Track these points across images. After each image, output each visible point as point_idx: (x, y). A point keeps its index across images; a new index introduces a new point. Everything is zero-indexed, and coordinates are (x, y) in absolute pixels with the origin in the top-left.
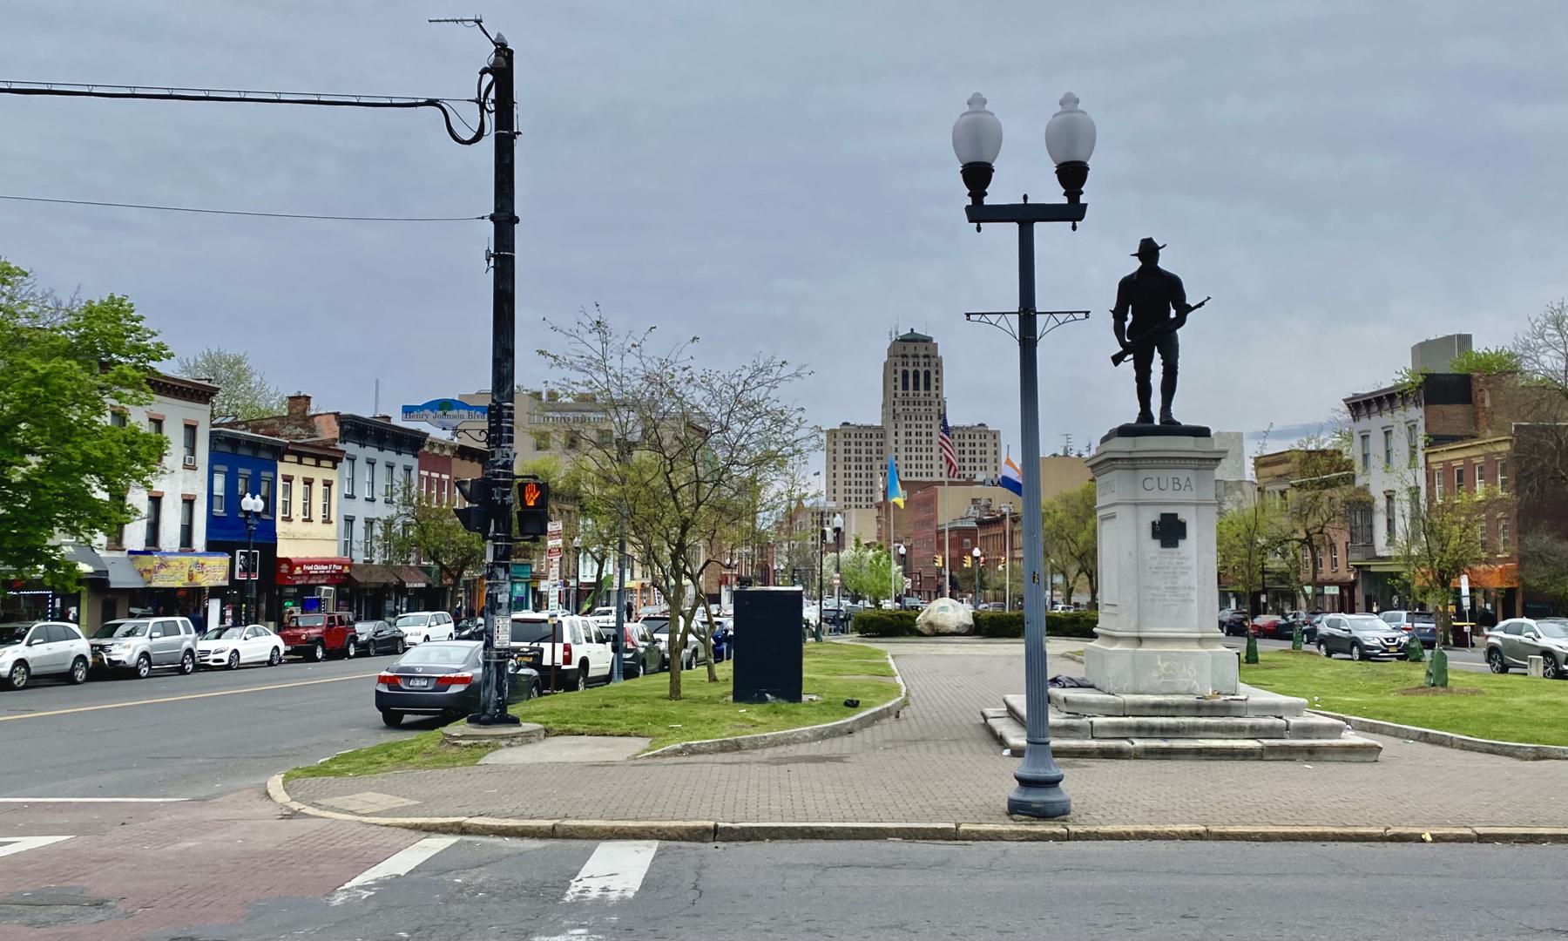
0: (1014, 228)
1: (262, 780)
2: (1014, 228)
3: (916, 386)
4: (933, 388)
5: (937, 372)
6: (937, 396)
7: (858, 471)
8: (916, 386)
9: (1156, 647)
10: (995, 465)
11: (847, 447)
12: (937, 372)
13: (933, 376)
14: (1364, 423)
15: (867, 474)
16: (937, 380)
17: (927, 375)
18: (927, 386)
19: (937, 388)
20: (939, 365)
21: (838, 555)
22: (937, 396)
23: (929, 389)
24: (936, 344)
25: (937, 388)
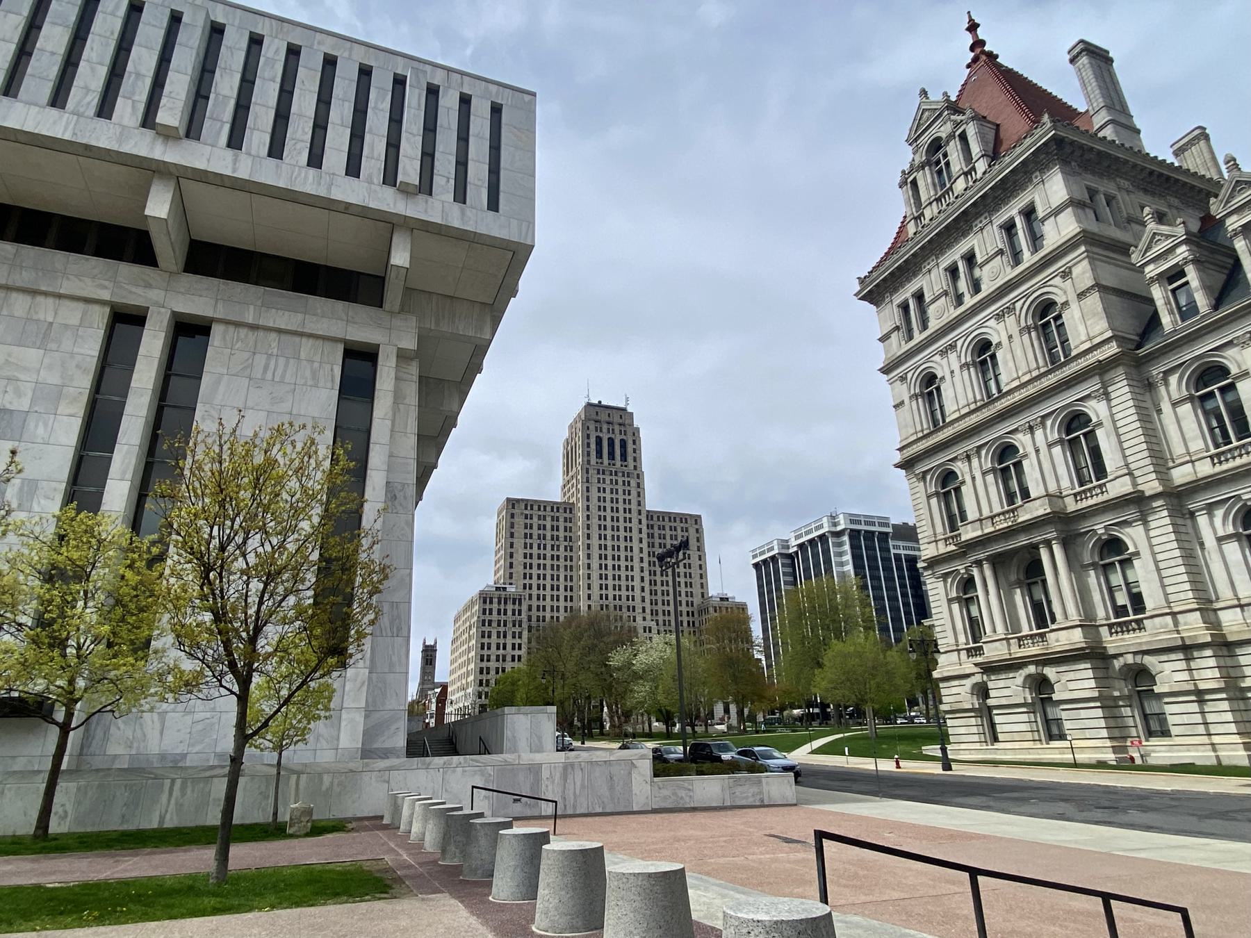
0: (200, 99)
1: (219, 841)
2: (200, 99)
3: (612, 455)
4: (630, 459)
5: (634, 442)
6: (635, 468)
7: (541, 603)
8: (612, 455)
9: (1062, 759)
10: (701, 591)
11: (528, 521)
12: (634, 442)
13: (630, 443)
14: (70, 104)
15: (531, 578)
16: (635, 451)
17: (623, 444)
18: (624, 457)
19: (635, 460)
20: (636, 432)
21: (57, 724)
22: (635, 468)
23: (613, 459)
24: (638, 429)
25: (635, 460)
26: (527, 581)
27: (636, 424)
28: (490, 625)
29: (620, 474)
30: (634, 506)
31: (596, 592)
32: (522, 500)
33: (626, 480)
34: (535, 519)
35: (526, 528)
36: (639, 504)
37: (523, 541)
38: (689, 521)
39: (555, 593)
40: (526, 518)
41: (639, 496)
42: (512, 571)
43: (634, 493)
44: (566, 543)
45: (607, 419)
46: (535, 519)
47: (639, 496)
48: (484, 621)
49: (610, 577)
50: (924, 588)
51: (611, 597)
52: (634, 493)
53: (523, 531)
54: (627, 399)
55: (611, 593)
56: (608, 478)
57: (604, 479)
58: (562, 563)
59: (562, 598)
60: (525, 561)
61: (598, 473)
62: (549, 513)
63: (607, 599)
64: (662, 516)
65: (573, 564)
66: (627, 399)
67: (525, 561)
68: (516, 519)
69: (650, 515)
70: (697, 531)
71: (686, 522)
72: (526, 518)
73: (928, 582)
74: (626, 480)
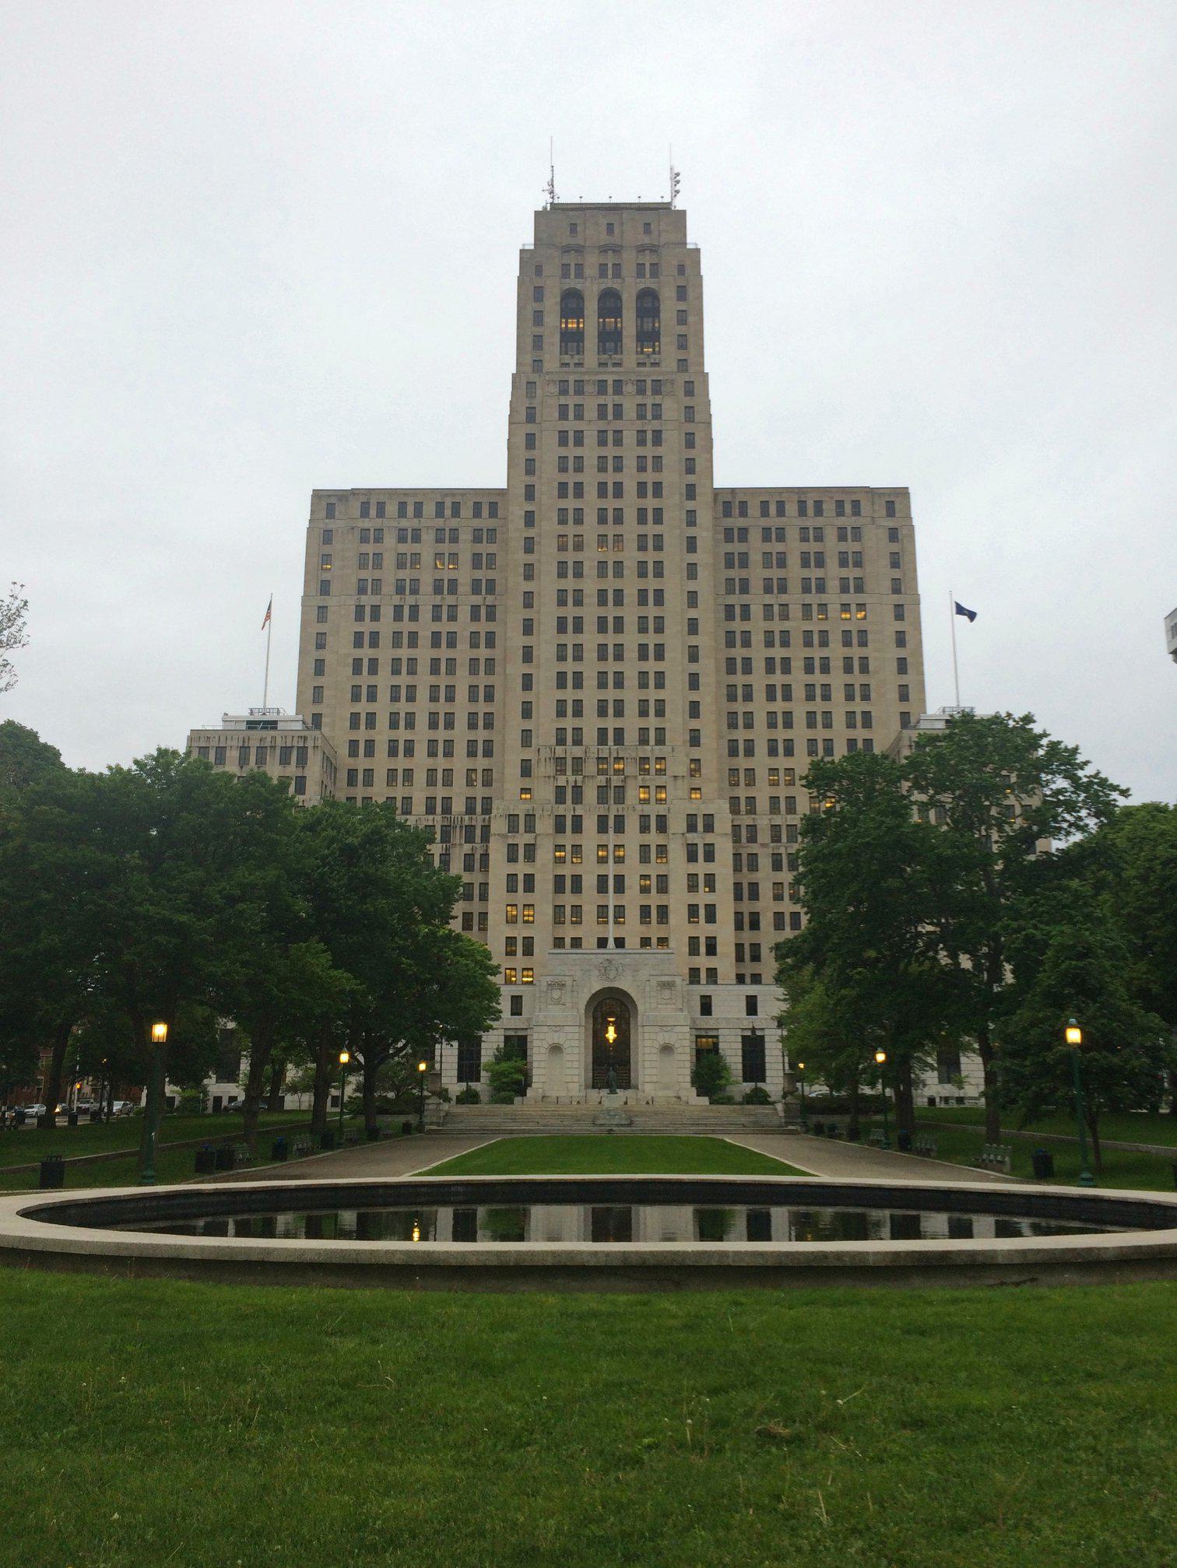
3: (610, 339)
4: (668, 343)
6: (683, 364)
17: (648, 305)
18: (648, 337)
22: (683, 364)
26: (363, 707)
27: (692, 239)
28: (577, 770)
29: (630, 388)
30: (672, 477)
31: (545, 724)
32: (354, 492)
33: (649, 400)
34: (390, 540)
35: (362, 565)
36: (690, 467)
37: (352, 602)
38: (865, 508)
39: (441, 734)
40: (364, 540)
41: (690, 443)
42: (320, 681)
43: (673, 438)
44: (477, 600)
45: (604, 238)
46: (390, 540)
47: (690, 443)
48: (487, 783)
49: (423, 694)
50: (511, 1264)
51: (590, 737)
52: (673, 438)
53: (353, 575)
54: (676, 178)
55: (590, 724)
56: (591, 404)
57: (579, 407)
58: (463, 653)
59: (461, 749)
60: (359, 653)
61: (564, 392)
62: (792, 521)
63: (577, 742)
64: (774, 501)
65: (496, 653)
66: (676, 178)
67: (359, 653)
68: (337, 545)
69: (733, 502)
70: (893, 535)
71: (856, 512)
72: (364, 540)
73: (688, 1042)
74: (649, 400)
